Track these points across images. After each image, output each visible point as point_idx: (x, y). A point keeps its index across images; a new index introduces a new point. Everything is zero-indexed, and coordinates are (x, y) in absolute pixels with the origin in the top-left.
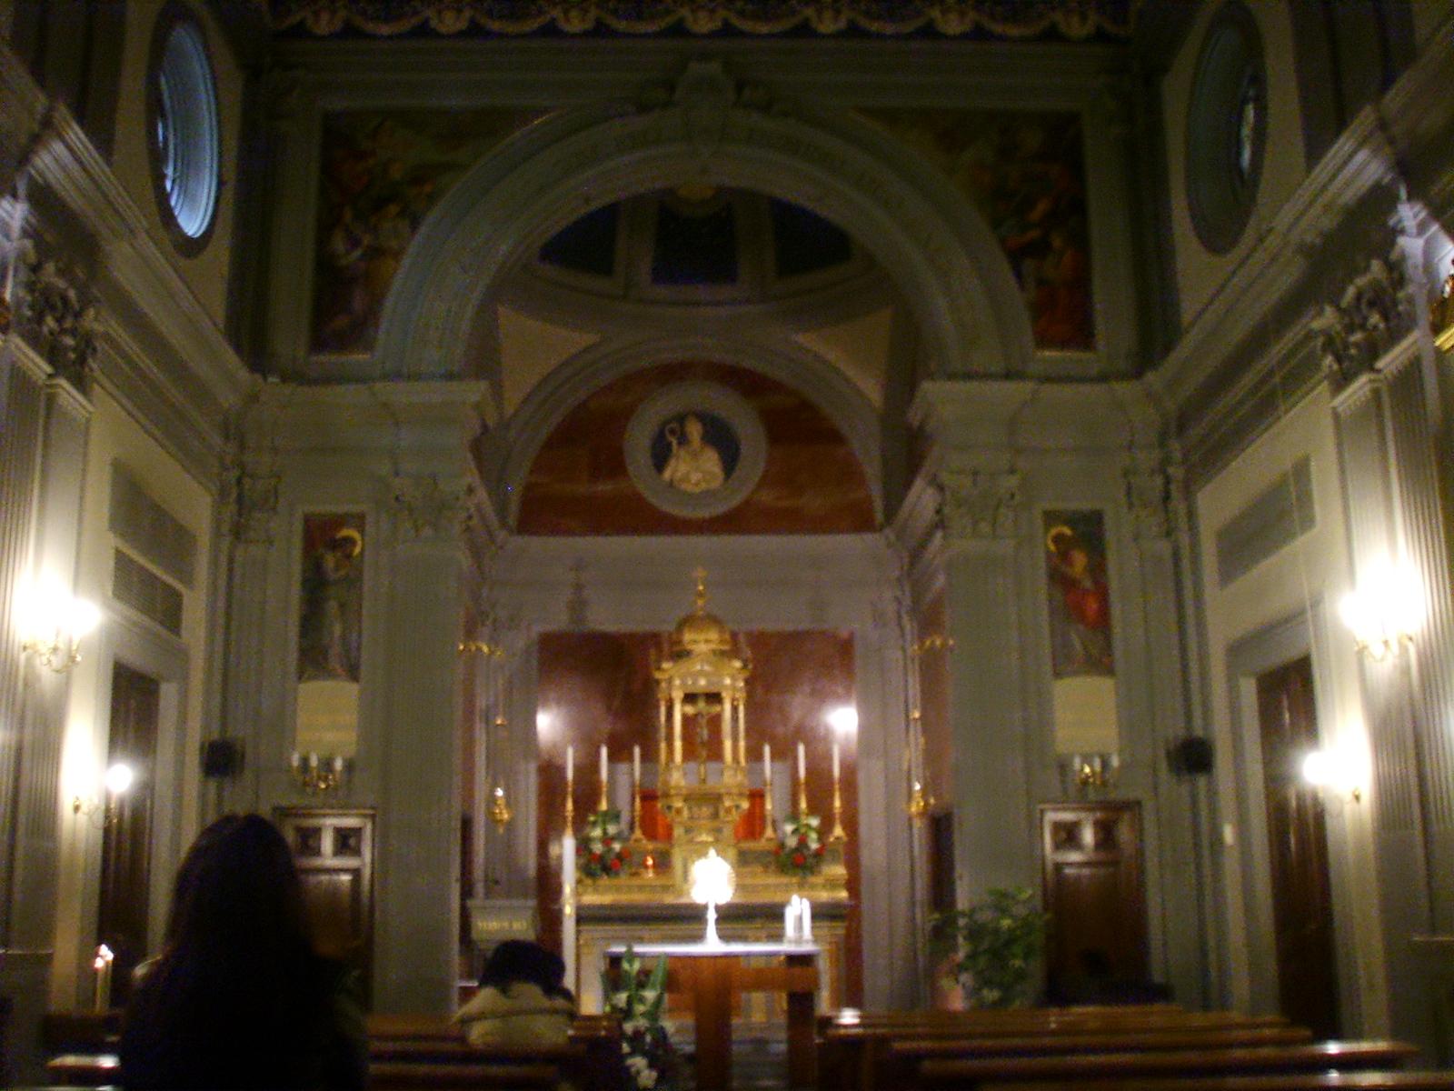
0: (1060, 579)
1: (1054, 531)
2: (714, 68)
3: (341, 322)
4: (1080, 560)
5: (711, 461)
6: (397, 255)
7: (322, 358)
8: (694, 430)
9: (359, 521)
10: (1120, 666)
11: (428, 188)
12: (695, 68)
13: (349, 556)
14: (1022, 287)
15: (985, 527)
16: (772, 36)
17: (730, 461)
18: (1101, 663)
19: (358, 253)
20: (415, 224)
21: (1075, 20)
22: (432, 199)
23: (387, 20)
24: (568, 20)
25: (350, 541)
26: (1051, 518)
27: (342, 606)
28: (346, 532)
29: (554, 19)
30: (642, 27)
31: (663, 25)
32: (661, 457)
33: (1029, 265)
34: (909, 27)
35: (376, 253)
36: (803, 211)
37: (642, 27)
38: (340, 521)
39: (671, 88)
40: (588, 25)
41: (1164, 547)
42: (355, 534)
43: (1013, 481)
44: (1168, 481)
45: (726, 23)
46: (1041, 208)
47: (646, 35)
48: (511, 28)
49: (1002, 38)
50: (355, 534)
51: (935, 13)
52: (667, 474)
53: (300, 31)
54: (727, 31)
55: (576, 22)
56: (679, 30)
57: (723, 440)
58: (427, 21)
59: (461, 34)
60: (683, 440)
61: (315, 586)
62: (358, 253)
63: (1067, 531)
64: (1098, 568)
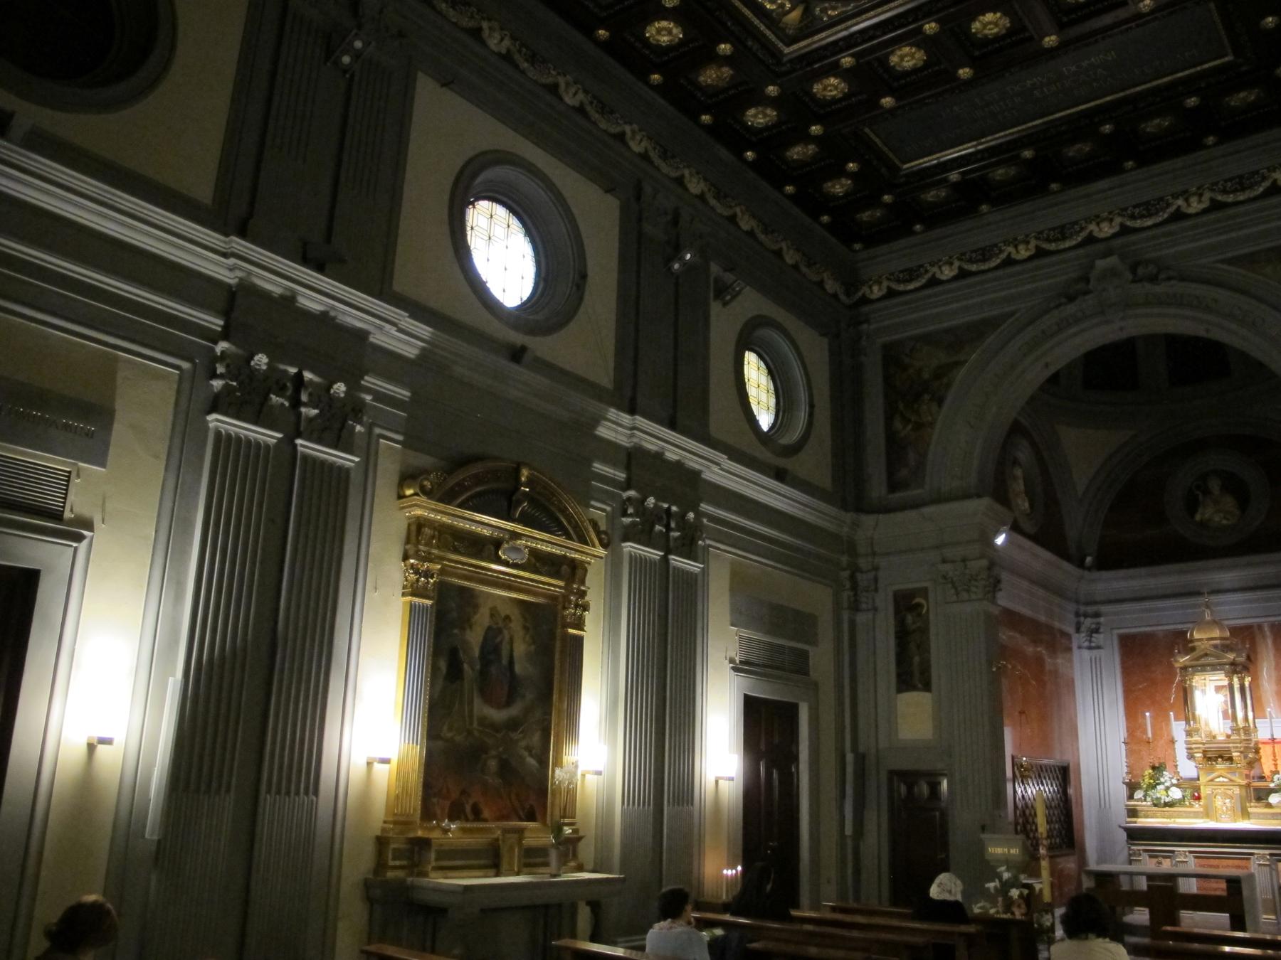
2: (1113, 260)
3: (904, 473)
5: (1229, 502)
6: (932, 425)
7: (898, 495)
8: (1215, 485)
9: (924, 592)
11: (945, 380)
12: (1101, 264)
13: (920, 615)
16: (1156, 226)
17: (1243, 501)
19: (910, 427)
20: (940, 402)
21: (1194, 200)
22: (948, 386)
23: (1150, 215)
24: (1189, 205)
25: (919, 605)
27: (918, 647)
28: (918, 600)
29: (1179, 207)
30: (1068, 244)
31: (1080, 239)
32: (1192, 505)
34: (923, 281)
35: (919, 426)
36: (1197, 339)
37: (1068, 244)
38: (912, 594)
39: (1087, 280)
40: (955, 272)
42: (923, 601)
45: (1122, 225)
47: (1070, 249)
48: (983, 267)
50: (923, 601)
52: (1198, 517)
53: (865, 301)
54: (1124, 231)
55: (1195, 204)
56: (1091, 240)
58: (934, 275)
59: (955, 278)
60: (1207, 492)
61: (903, 635)
62: (910, 427)
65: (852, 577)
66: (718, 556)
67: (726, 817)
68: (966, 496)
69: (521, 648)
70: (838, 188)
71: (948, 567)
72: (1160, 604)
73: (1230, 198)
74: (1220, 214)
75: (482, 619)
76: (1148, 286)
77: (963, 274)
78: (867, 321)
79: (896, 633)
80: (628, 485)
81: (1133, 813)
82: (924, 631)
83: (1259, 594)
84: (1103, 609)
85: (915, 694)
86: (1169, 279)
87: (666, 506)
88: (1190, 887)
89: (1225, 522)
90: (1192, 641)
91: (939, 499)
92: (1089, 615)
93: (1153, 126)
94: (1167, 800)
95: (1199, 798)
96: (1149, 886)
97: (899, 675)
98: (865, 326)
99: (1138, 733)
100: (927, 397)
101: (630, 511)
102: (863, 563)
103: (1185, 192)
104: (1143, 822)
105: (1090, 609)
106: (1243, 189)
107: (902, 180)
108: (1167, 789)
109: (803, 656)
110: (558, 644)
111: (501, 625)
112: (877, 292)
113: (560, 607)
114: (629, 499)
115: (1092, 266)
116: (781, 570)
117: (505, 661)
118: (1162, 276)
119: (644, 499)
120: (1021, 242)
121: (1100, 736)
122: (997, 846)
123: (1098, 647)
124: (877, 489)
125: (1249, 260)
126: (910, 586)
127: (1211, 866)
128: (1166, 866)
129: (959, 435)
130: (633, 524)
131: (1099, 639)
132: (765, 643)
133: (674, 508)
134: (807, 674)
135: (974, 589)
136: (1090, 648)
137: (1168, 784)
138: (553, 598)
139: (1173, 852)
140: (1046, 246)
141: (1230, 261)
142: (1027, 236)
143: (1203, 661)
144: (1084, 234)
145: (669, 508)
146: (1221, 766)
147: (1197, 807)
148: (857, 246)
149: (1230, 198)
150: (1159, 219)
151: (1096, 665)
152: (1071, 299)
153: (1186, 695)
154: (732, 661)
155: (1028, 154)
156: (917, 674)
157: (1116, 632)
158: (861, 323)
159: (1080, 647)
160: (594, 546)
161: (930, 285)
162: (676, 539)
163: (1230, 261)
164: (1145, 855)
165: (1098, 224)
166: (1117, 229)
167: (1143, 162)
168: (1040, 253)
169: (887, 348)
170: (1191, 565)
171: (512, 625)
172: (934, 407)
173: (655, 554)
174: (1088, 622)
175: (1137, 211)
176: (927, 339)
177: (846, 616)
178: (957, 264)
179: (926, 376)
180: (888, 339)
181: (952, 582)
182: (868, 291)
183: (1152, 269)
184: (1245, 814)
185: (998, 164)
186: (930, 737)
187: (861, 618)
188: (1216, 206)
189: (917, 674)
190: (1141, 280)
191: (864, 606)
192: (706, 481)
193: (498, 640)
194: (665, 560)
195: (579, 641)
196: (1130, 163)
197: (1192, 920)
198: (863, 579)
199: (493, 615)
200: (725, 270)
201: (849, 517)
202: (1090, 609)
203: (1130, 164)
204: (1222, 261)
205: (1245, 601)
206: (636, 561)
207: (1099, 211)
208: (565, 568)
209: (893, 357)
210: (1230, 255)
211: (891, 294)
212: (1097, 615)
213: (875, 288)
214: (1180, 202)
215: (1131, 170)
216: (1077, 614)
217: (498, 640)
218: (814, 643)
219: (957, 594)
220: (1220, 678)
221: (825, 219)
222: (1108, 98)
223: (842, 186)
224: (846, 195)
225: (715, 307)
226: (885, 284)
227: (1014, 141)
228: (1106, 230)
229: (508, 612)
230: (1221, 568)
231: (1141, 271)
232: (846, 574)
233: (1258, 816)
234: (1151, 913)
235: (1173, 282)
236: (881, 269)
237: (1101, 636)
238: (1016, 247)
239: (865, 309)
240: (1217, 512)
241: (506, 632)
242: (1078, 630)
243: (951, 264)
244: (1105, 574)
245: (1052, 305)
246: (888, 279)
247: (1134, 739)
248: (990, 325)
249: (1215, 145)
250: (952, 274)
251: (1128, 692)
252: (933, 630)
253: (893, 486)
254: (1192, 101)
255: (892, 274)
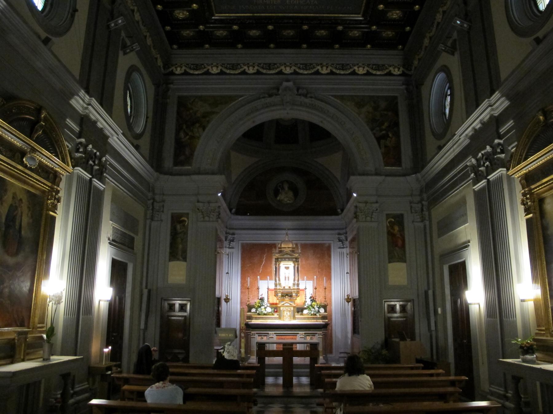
0: (390, 234)
1: (389, 220)
2: (290, 84)
3: (182, 158)
4: (396, 228)
5: (291, 194)
6: (198, 138)
7: (176, 168)
8: (286, 186)
9: (187, 215)
10: (188, 260)
11: (207, 119)
12: (285, 84)
13: (184, 225)
14: (380, 148)
15: (368, 218)
16: (307, 74)
18: (402, 259)
19: (188, 137)
20: (204, 128)
21: (396, 70)
22: (208, 122)
23: (306, 70)
25: (184, 221)
26: (388, 216)
27: (182, 240)
28: (183, 218)
32: (277, 193)
33: (382, 141)
35: (192, 138)
38: (182, 215)
39: (278, 90)
41: (421, 225)
42: (186, 219)
43: (377, 205)
44: (423, 205)
46: (386, 124)
48: (232, 72)
49: (375, 75)
51: (356, 68)
52: (278, 198)
54: (295, 73)
55: (251, 70)
56: (281, 73)
57: (295, 190)
58: (245, 70)
59: (254, 74)
60: (283, 189)
61: (174, 234)
62: (188, 137)
63: (393, 220)
64: (402, 229)
65: (153, 204)
66: (108, 183)
67: (101, 321)
68: (213, 173)
69: (25, 220)
70: (181, 14)
71: (201, 205)
72: (259, 232)
73: (338, 72)
74: (333, 77)
75: (8, 198)
76: (303, 98)
77: (222, 73)
78: (172, 83)
79: (171, 233)
80: (80, 136)
81: (250, 318)
82: (186, 233)
83: (301, 232)
84: (236, 232)
85: (178, 262)
86: (311, 97)
87: (95, 151)
88: (299, 347)
89: (288, 202)
90: (280, 248)
91: (199, 173)
92: (230, 235)
93: (254, 33)
94: (265, 312)
95: (277, 312)
96: (283, 348)
97: (170, 253)
98: (171, 86)
99: (245, 285)
100: (197, 125)
101: (81, 150)
102: (157, 198)
103: (321, 64)
104: (254, 322)
105: (231, 231)
106: (343, 70)
107: (213, 21)
108: (265, 308)
109: (132, 239)
110: (43, 218)
111: (17, 205)
112: (179, 71)
113: (46, 198)
114: (81, 143)
115: (281, 84)
116: (130, 196)
117: (17, 227)
118: (308, 96)
119: (87, 146)
120: (251, 66)
121: (231, 286)
122: (221, 333)
123: (233, 248)
124: (168, 163)
125: (342, 98)
126: (181, 211)
127: (282, 339)
128: (265, 339)
129: (211, 145)
130: (81, 158)
131: (233, 244)
132: (122, 231)
133: (98, 153)
134: (133, 248)
135: (211, 216)
136: (229, 248)
137: (266, 306)
138: (44, 192)
139: (268, 333)
140: (261, 70)
141: (335, 96)
142: (254, 64)
143: (285, 256)
144: (278, 70)
145: (96, 153)
146: (287, 299)
147: (276, 315)
148: (175, 47)
149: (228, 71)
150: (310, 72)
151: (342, 254)
152: (270, 96)
153: (277, 270)
154: (109, 239)
155: (235, 27)
156: (180, 253)
157: (240, 242)
158: (170, 84)
159: (226, 247)
160: (68, 165)
161: (207, 74)
162: (97, 170)
163: (335, 96)
164: (257, 335)
165: (285, 67)
166: (255, 71)
167: (374, 46)
168: (258, 73)
169: (179, 97)
170: (275, 217)
171: (23, 205)
172: (201, 130)
173: (87, 176)
174: (230, 237)
175: (301, 66)
176: (201, 98)
177: (148, 222)
178: (184, 68)
179: (199, 115)
180: (181, 94)
181: (202, 212)
182: (175, 69)
183: (304, 91)
184: (294, 318)
185: (219, 28)
186: (184, 282)
187: (154, 224)
188: (332, 73)
189: (180, 253)
190: (300, 95)
191: (156, 219)
192: (110, 144)
193: (15, 213)
194: (91, 180)
195: (53, 219)
196: (337, 46)
197: (297, 360)
198: (157, 206)
199: (14, 197)
200: (126, 37)
201: (156, 174)
202: (231, 231)
203: (305, 46)
204: (332, 96)
205: (295, 234)
206: (80, 178)
207: (287, 61)
208: (51, 175)
209: (182, 103)
210: (334, 94)
211: (186, 73)
212: (233, 234)
213: (179, 69)
214: (319, 67)
215: (337, 49)
216: (226, 233)
217: (15, 213)
218: (137, 235)
219: (204, 218)
220: (291, 265)
221: (168, 28)
222: (312, 15)
223: (397, 14)
224: (183, 19)
225: (121, 53)
226: (184, 68)
227: (231, 20)
228: (288, 70)
229: (21, 197)
230: (286, 220)
231: (300, 91)
232: (150, 202)
233: (299, 319)
234: (283, 359)
235: (313, 99)
236: (183, 61)
237: (234, 243)
238: (248, 67)
239: (172, 77)
240: (286, 197)
241: (19, 209)
242: (226, 240)
243: (217, 67)
244: (240, 217)
245: (261, 96)
246: (185, 66)
247: (245, 288)
248: (231, 99)
249: (241, 48)
250: (217, 72)
251: (242, 267)
252: (189, 232)
253: (176, 164)
254: (270, 27)
255: (188, 64)
